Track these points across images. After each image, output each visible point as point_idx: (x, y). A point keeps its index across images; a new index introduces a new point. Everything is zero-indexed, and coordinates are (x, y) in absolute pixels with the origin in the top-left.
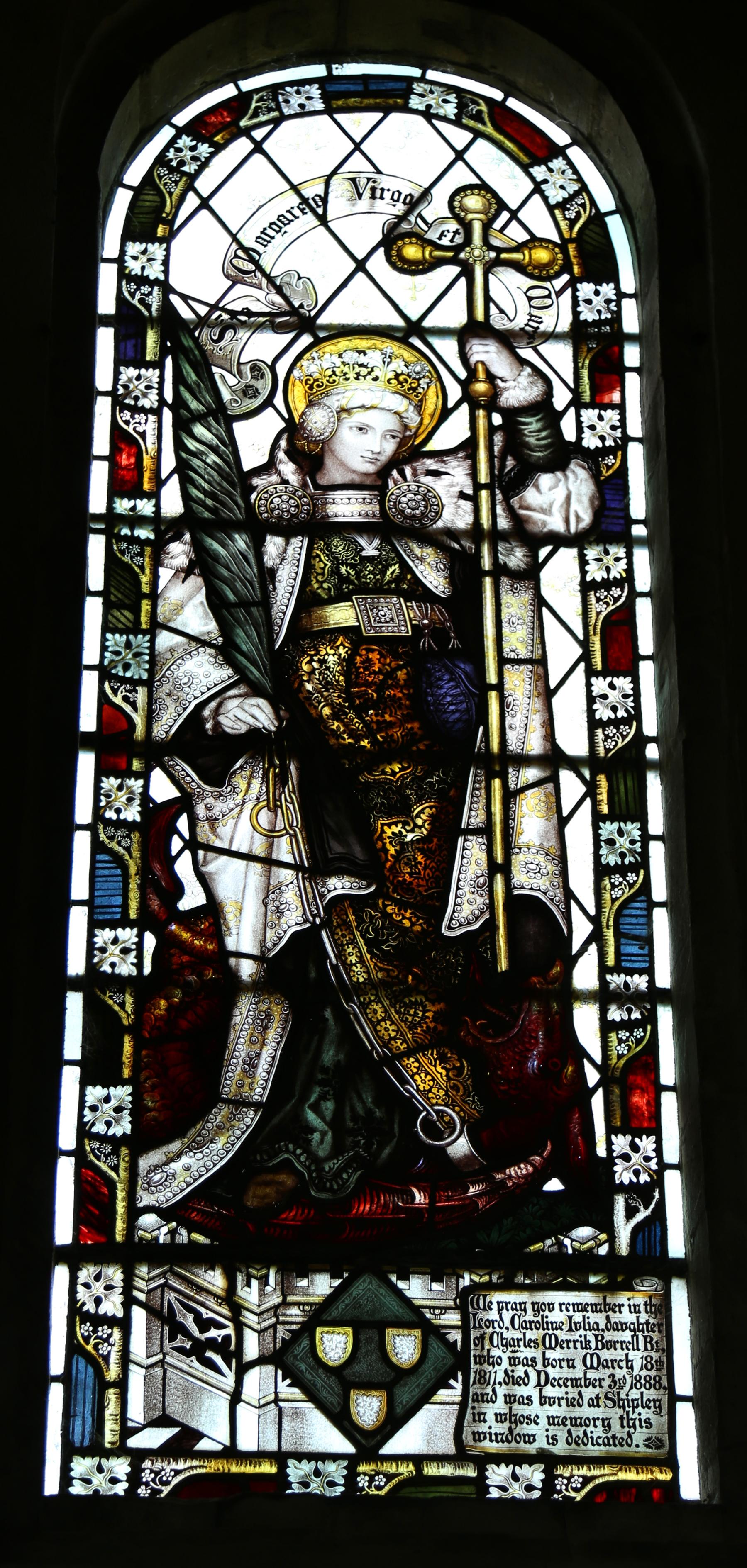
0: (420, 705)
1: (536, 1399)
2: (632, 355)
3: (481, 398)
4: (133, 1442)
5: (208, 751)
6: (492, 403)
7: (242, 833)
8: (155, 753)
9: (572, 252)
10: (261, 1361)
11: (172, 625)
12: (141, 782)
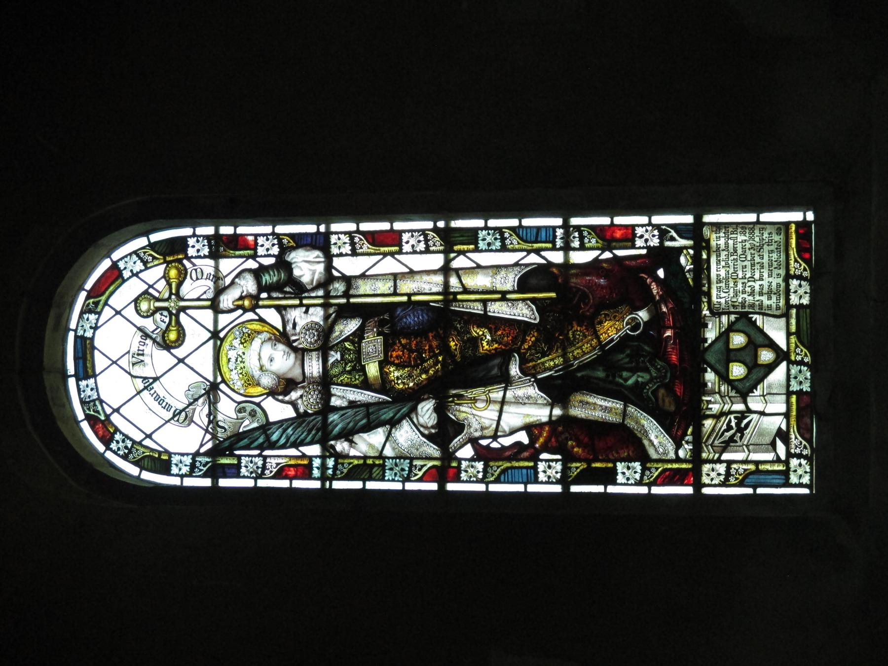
0: (420, 333)
1: (761, 282)
2: (226, 230)
3: (255, 302)
4: (783, 457)
5: (446, 431)
6: (256, 298)
7: (488, 416)
8: (448, 456)
9: (171, 258)
11: (380, 449)
12: (463, 462)
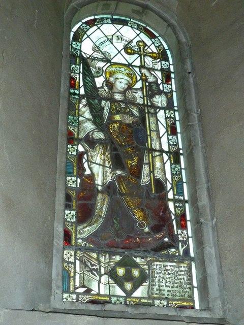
1: (165, 286)
2: (173, 76)
3: (144, 79)
5: (91, 142)
7: (98, 159)
8: (79, 141)
10: (105, 274)
